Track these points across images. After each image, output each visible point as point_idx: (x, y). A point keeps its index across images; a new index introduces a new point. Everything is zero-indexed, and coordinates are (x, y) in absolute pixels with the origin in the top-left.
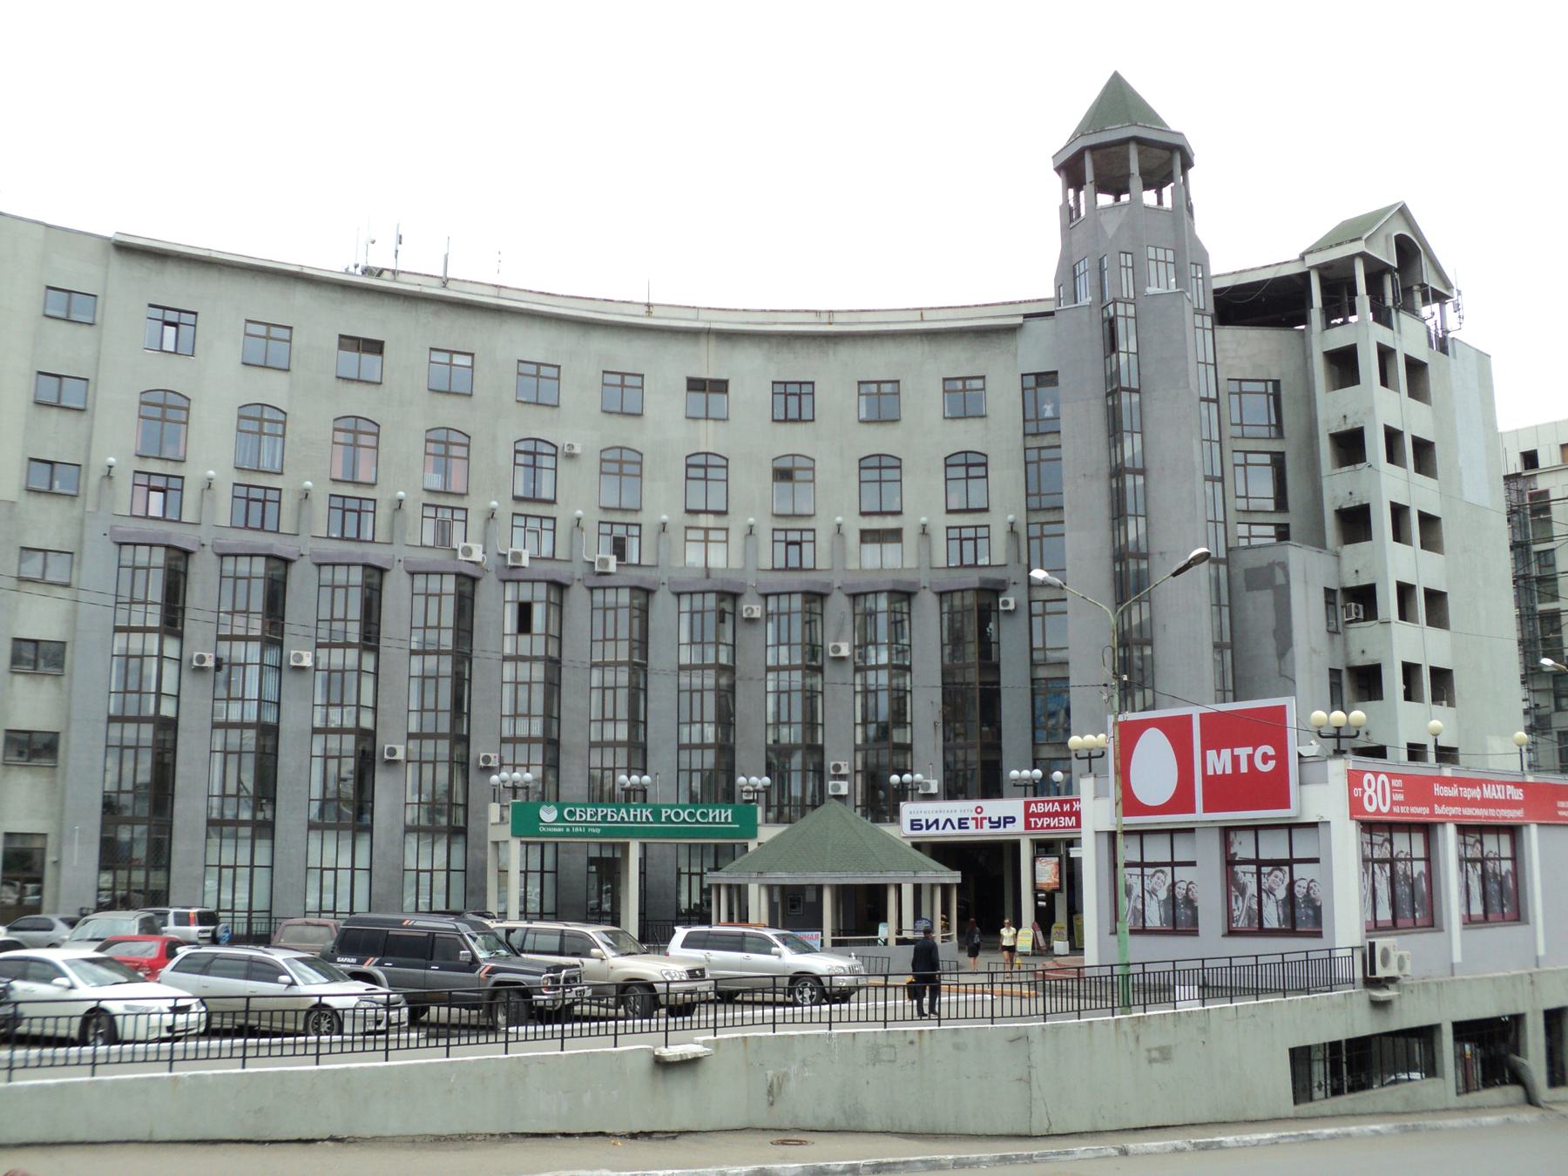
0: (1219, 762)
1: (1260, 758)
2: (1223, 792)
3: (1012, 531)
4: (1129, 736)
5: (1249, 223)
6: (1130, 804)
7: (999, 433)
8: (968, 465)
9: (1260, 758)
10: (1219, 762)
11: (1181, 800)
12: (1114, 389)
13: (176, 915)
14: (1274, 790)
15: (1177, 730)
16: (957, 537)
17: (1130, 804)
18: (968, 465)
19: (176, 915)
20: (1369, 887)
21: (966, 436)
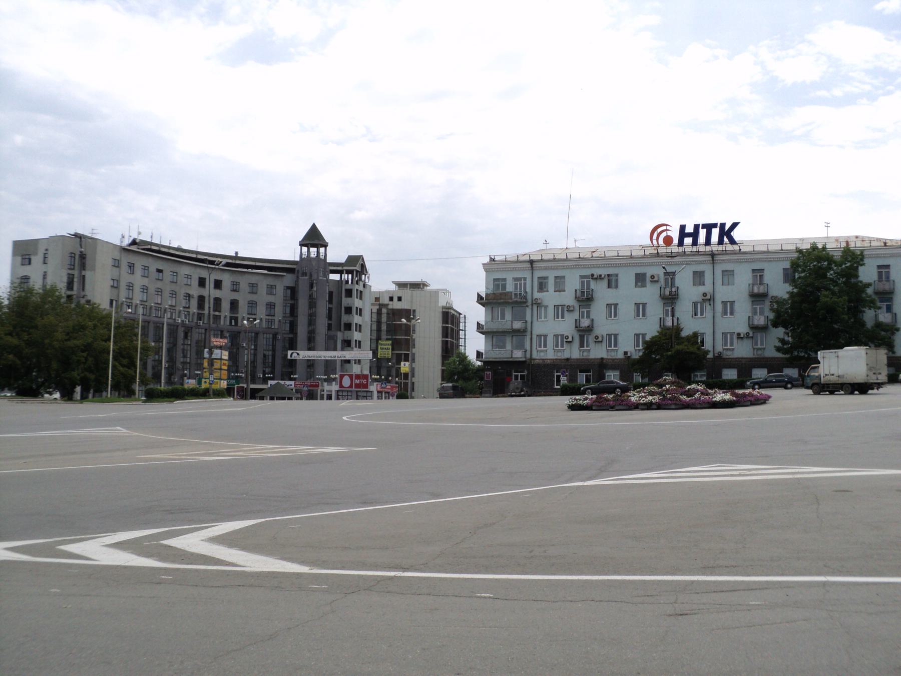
0: (358, 381)
1: (364, 382)
2: (357, 386)
3: (280, 321)
4: (342, 377)
5: (335, 254)
6: (341, 386)
7: (279, 297)
8: (271, 306)
9: (364, 382)
10: (358, 381)
11: (351, 386)
12: (311, 296)
13: (214, 311)
14: (366, 386)
15: (351, 376)
16: (268, 321)
17: (341, 386)
18: (271, 306)
19: (214, 311)
20: (685, 612)
21: (271, 299)
